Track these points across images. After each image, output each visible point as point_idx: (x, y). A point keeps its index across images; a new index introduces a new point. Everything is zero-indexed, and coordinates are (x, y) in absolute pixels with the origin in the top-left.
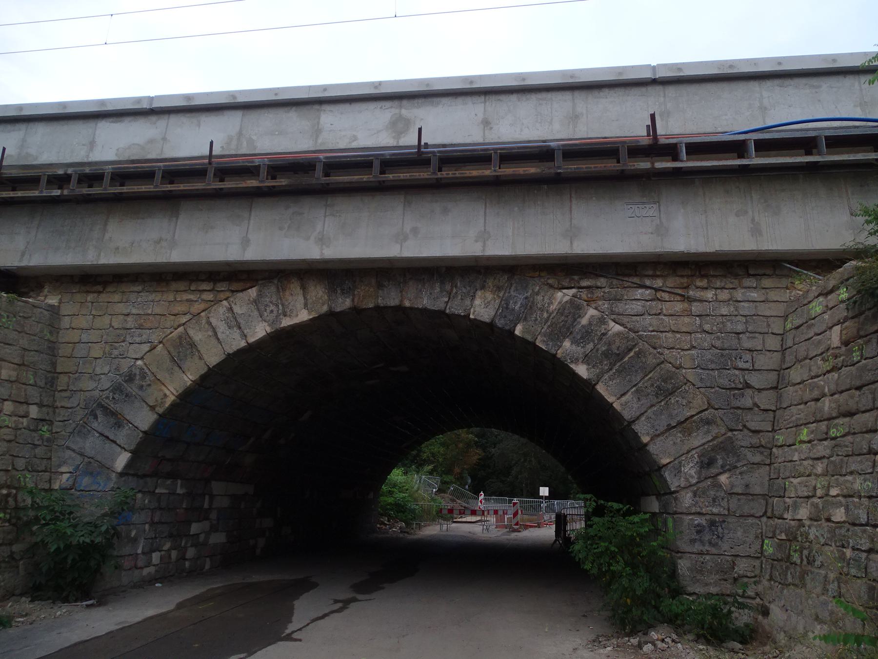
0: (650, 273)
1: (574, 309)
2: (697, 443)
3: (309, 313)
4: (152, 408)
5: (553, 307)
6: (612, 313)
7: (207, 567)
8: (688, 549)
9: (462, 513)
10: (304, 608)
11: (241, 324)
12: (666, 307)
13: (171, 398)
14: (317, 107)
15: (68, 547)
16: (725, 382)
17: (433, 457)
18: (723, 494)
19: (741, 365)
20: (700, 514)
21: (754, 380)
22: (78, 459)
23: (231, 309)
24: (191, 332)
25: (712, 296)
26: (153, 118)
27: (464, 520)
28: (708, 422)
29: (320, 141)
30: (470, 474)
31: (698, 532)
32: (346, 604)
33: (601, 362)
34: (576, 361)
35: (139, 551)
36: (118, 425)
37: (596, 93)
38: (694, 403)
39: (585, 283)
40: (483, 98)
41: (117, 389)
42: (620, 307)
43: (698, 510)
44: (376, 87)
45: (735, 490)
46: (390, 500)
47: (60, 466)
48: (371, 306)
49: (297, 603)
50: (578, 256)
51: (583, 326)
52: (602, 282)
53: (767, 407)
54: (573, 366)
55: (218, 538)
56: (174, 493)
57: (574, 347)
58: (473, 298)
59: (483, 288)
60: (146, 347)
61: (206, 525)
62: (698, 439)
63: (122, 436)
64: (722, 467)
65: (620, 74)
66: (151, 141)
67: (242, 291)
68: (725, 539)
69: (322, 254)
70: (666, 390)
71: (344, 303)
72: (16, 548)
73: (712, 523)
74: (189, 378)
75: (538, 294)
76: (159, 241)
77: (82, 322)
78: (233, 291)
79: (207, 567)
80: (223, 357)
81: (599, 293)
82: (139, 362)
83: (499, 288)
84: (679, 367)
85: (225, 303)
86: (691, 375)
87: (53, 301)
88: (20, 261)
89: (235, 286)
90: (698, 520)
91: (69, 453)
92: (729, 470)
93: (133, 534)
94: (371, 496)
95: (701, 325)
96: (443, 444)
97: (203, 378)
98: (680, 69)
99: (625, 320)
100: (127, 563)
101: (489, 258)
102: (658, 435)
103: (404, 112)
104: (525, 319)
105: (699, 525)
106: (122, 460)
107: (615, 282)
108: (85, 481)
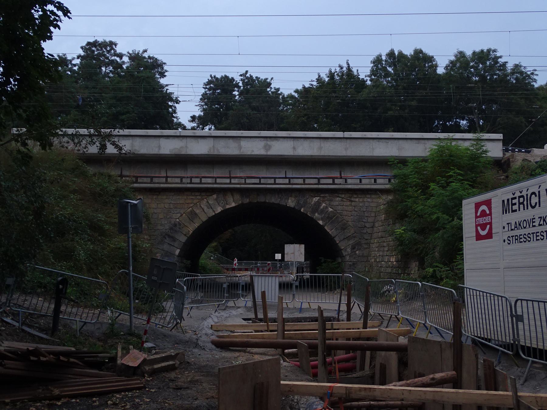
1: (318, 204)
4: (185, 235)
6: (330, 205)
12: (345, 203)
19: (364, 221)
21: (367, 225)
23: (208, 202)
24: (195, 210)
25: (357, 200)
26: (181, 138)
28: (355, 237)
29: (242, 151)
34: (319, 220)
37: (327, 140)
39: (322, 195)
41: (171, 229)
42: (332, 203)
52: (327, 195)
58: (288, 199)
59: (291, 196)
60: (179, 215)
62: (351, 242)
63: (176, 244)
66: (182, 147)
71: (247, 201)
73: (354, 264)
74: (197, 225)
81: (326, 199)
82: (177, 220)
84: (348, 221)
86: (350, 223)
90: (350, 263)
106: (177, 252)
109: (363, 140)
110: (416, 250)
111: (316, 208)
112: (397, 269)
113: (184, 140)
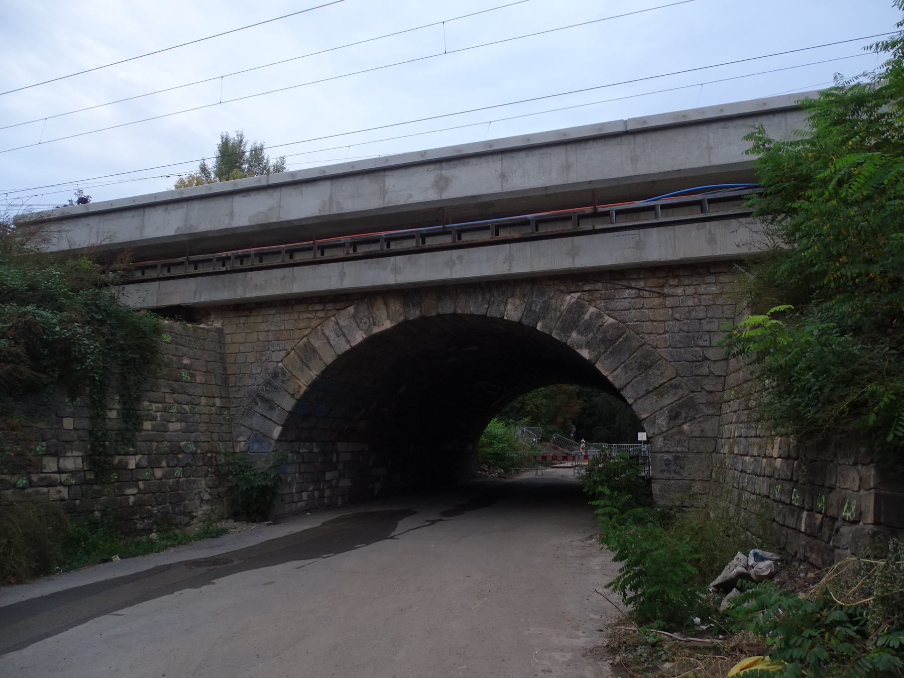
0: (636, 277)
1: (579, 308)
2: (667, 402)
3: (392, 322)
4: (292, 395)
5: (563, 308)
6: (607, 309)
7: (340, 502)
8: (659, 476)
9: (565, 458)
10: (402, 525)
11: (345, 334)
12: (647, 303)
13: (304, 388)
14: (382, 173)
15: (252, 488)
16: (689, 357)
17: (537, 408)
18: (684, 438)
19: (701, 343)
20: (668, 452)
21: (711, 354)
22: (249, 433)
23: (337, 323)
24: (312, 341)
25: (682, 292)
26: (271, 191)
27: (566, 465)
28: (676, 387)
29: (386, 199)
30: (573, 422)
31: (666, 465)
32: (433, 522)
33: (599, 347)
34: (581, 347)
35: (294, 491)
36: (272, 408)
37: (583, 145)
38: (664, 374)
39: (587, 288)
40: (500, 156)
41: (268, 383)
42: (613, 304)
43: (667, 449)
44: (422, 156)
45: (694, 435)
46: (489, 450)
47: (238, 437)
48: (434, 314)
49: (400, 523)
50: (578, 269)
51: (586, 321)
52: (599, 286)
53: (720, 374)
54: (578, 351)
55: (346, 483)
56: (311, 452)
57: (579, 337)
58: (506, 304)
59: (513, 296)
60: (283, 353)
61: (336, 473)
62: (668, 400)
63: (275, 415)
64: (685, 418)
65: (600, 129)
66: (271, 209)
67: (343, 309)
68: (686, 467)
69: (396, 280)
70: (646, 365)
71: (415, 314)
72: (220, 489)
73: (677, 458)
74: (314, 374)
75: (552, 298)
76: (283, 279)
77: (239, 338)
78: (337, 310)
79: (340, 502)
80: (335, 358)
81: (598, 295)
82: (280, 364)
83: (524, 296)
84: (656, 347)
85: (333, 318)
86: (664, 352)
87: (218, 324)
88: (194, 298)
89: (338, 306)
90: (666, 456)
91: (242, 428)
92: (690, 421)
93: (289, 479)
94: (470, 447)
95: (672, 315)
96: (545, 396)
97: (324, 372)
98: (645, 122)
99: (616, 314)
100: (287, 499)
101: (515, 275)
102: (640, 398)
103: (444, 172)
104: (544, 318)
105: (667, 460)
106: (277, 432)
107: (609, 285)
108: (256, 446)
109: (681, 131)
110: (857, 408)
111: (572, 320)
112: (787, 486)
113: (276, 194)
